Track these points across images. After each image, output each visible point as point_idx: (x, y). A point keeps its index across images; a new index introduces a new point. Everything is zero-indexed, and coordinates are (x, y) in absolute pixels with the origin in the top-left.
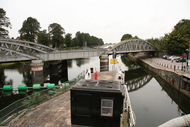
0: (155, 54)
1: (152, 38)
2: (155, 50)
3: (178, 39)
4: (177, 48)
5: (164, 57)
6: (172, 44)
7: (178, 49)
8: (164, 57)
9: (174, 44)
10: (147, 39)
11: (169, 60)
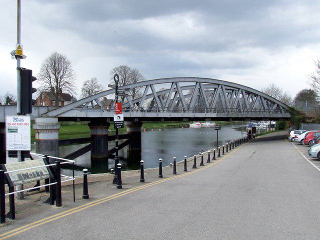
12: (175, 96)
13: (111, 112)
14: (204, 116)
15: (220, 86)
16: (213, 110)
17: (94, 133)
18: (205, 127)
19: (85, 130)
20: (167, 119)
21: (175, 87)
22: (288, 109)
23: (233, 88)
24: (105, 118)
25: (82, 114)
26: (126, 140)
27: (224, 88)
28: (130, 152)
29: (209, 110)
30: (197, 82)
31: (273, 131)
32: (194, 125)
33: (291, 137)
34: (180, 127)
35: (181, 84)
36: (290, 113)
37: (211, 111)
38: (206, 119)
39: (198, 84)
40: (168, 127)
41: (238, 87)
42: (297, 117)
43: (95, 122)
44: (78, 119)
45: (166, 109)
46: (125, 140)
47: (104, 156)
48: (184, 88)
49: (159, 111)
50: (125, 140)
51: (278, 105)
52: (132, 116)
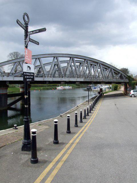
12: (54, 68)
14: (61, 80)
15: (99, 64)
16: (50, 75)
18: (66, 89)
20: (50, 82)
21: (56, 61)
22: (127, 76)
23: (95, 63)
24: (6, 81)
26: (20, 97)
27: (101, 66)
28: (23, 105)
29: (79, 76)
30: (71, 58)
31: (111, 91)
32: (60, 88)
33: (131, 95)
34: (51, 89)
35: (60, 59)
36: (129, 79)
37: (80, 77)
38: (102, 83)
39: (72, 59)
40: (44, 89)
41: (109, 66)
42: (133, 82)
45: (50, 75)
47: (5, 108)
49: (45, 77)
51: (121, 74)
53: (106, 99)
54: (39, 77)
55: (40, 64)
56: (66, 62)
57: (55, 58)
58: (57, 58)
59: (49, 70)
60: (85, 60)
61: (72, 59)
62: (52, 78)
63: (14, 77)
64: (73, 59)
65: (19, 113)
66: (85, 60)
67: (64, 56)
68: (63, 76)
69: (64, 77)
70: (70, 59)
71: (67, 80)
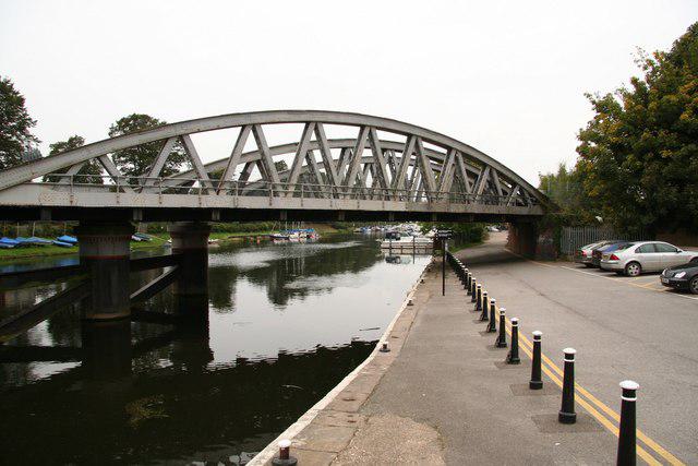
0: (541, 239)
1: (562, 170)
2: (537, 211)
3: (684, 116)
4: (680, 182)
5: (588, 250)
6: (640, 155)
7: (690, 190)
8: (588, 250)
9: (658, 157)
10: (652, 58)
11: (622, 273)
13: (144, 194)
16: (292, 189)
17: (92, 253)
19: (65, 246)
21: (314, 138)
25: (59, 198)
30: (363, 127)
36: (542, 206)
41: (517, 180)
43: (89, 222)
44: (44, 214)
45: (350, 192)
46: (167, 270)
48: (277, 151)
49: (276, 194)
50: (167, 270)
52: (204, 206)
53: (489, 271)
54: (247, 195)
55: (256, 148)
56: (337, 144)
57: (312, 127)
58: (316, 129)
59: (229, 155)
60: (410, 136)
61: (367, 131)
62: (380, 202)
63: (164, 193)
64: (370, 133)
65: (170, 328)
66: (450, 149)
67: (342, 119)
68: (339, 191)
69: (282, 195)
70: (361, 133)
71: (400, 206)
